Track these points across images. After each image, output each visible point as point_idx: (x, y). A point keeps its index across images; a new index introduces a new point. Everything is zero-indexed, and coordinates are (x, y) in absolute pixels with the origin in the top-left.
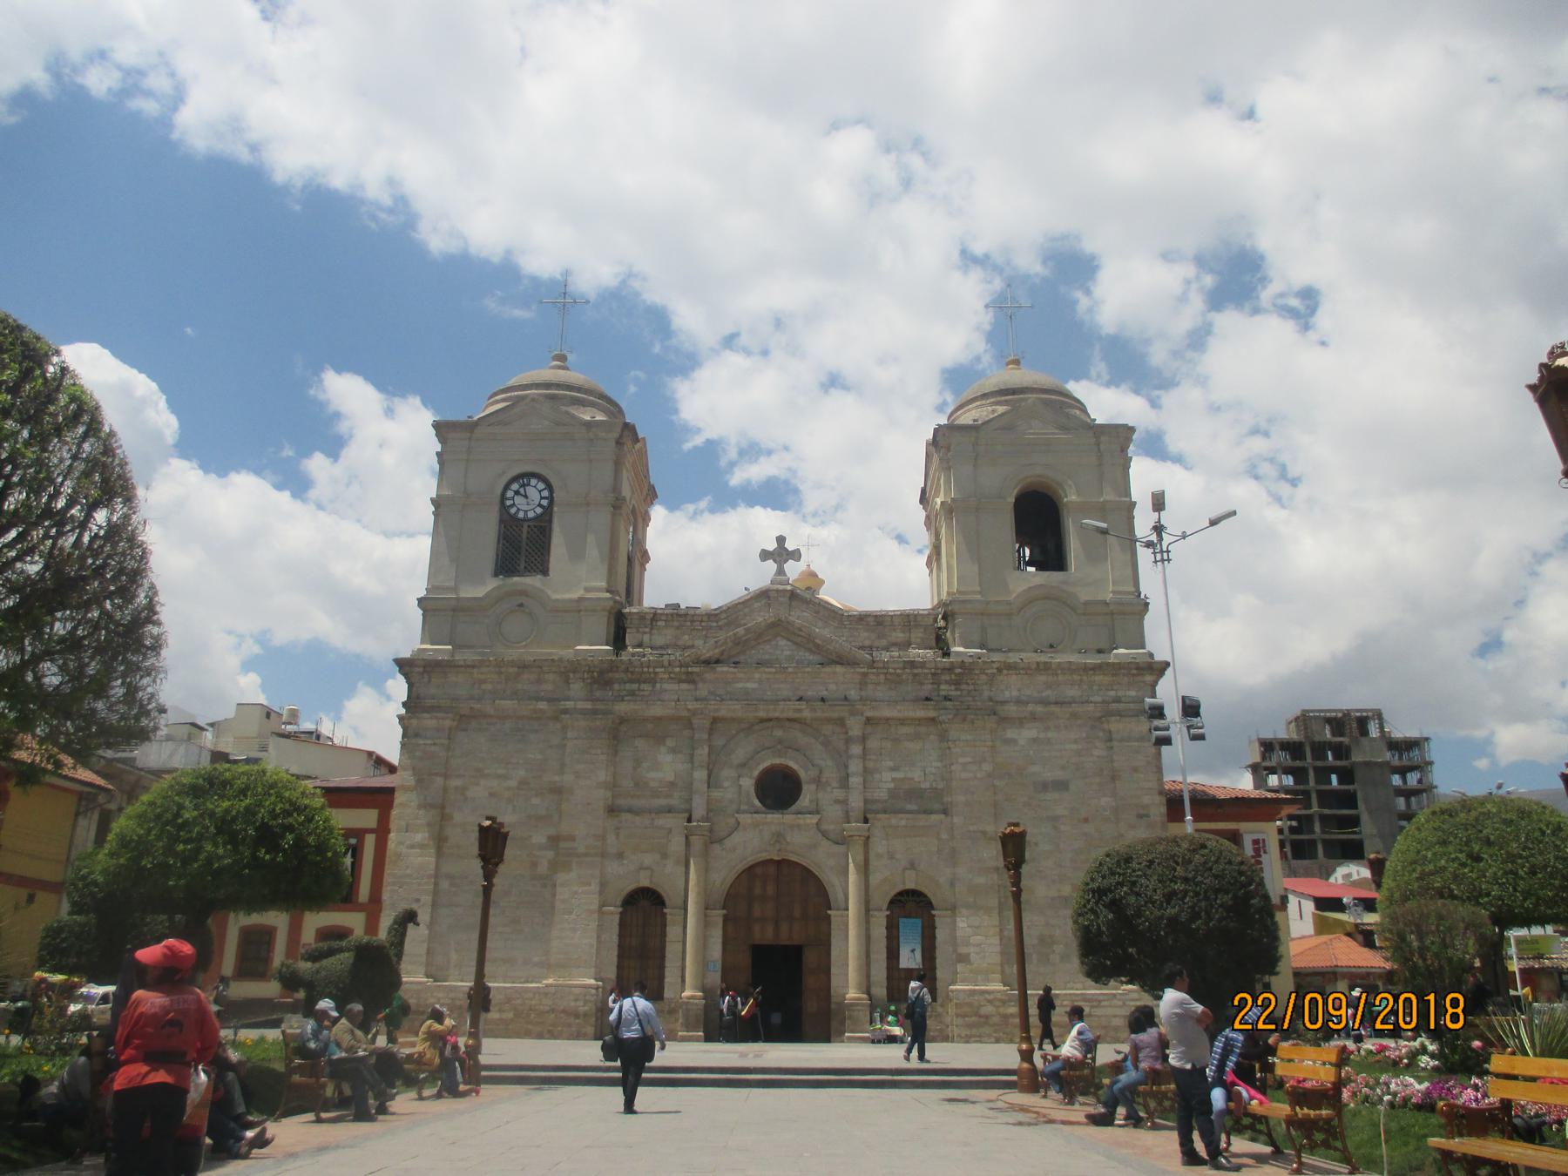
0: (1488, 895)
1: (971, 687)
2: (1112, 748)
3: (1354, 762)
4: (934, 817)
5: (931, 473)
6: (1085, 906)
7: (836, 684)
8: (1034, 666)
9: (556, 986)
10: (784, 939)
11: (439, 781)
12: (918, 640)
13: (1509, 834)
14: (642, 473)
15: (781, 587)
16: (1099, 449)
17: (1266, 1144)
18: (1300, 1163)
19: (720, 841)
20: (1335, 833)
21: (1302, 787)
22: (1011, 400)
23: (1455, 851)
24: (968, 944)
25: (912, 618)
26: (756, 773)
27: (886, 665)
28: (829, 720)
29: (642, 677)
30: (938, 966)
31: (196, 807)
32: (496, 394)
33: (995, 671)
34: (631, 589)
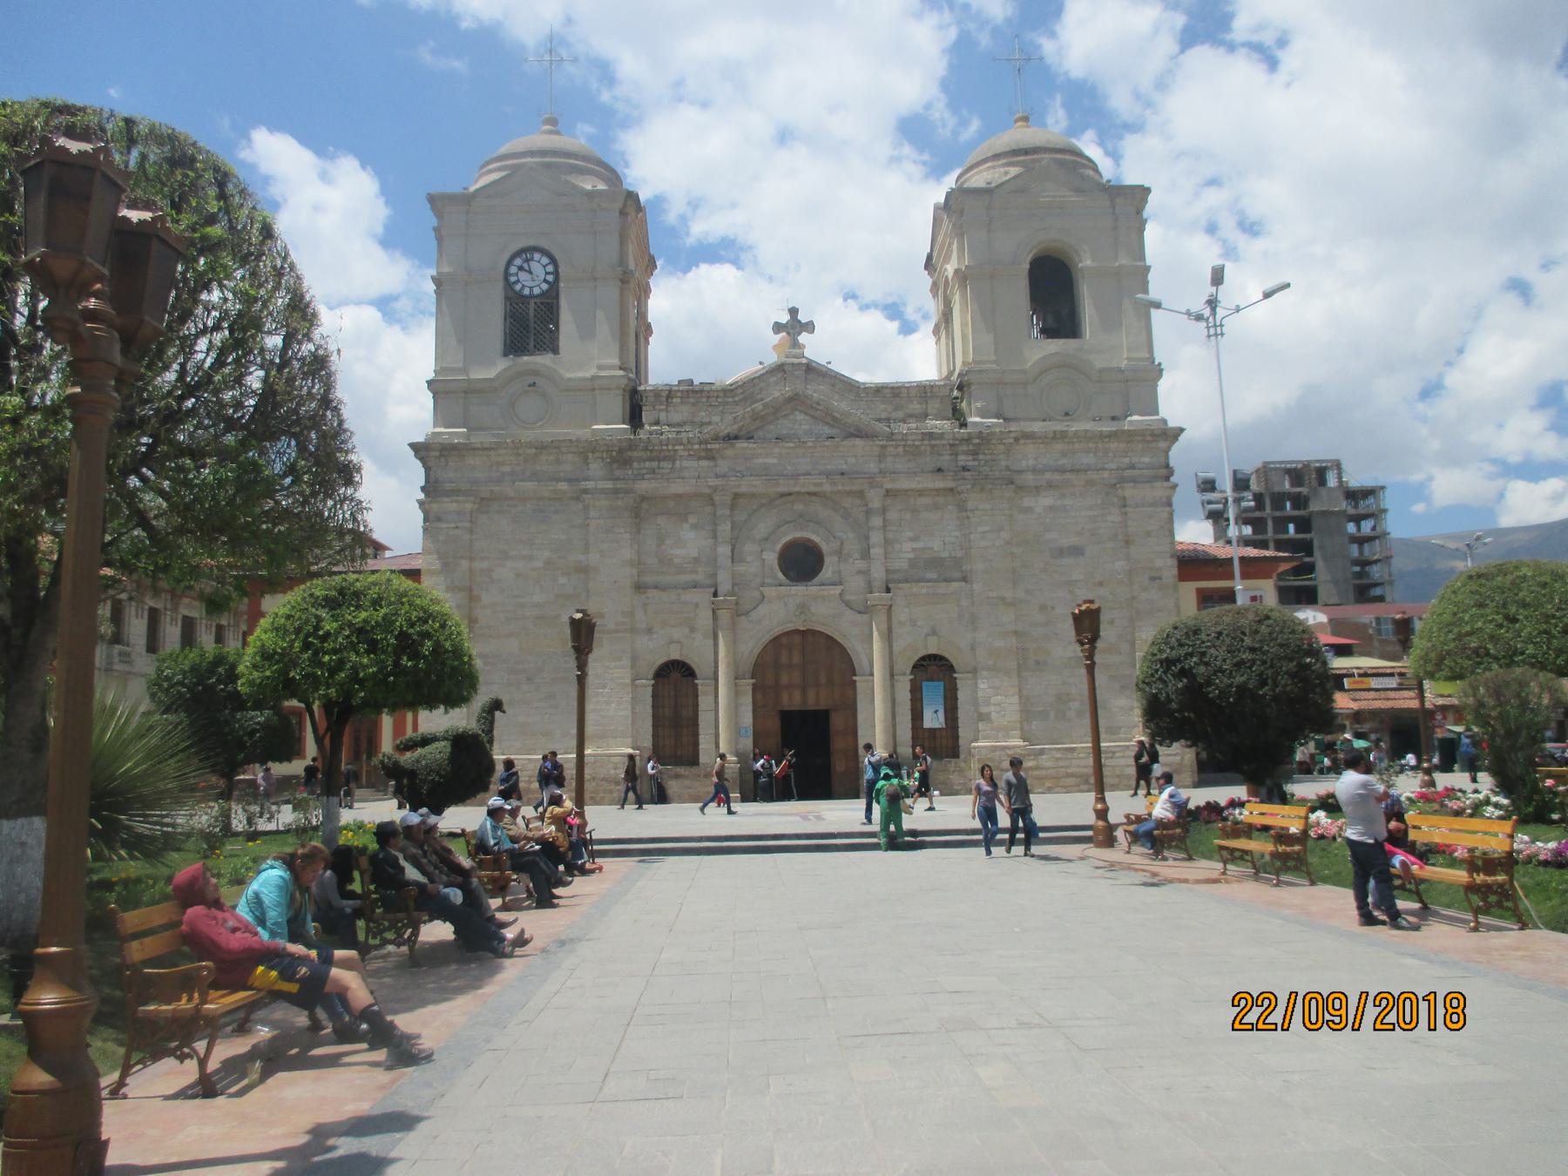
0: (1522, 653)
2: (1126, 514)
3: (1312, 512)
4: (955, 585)
5: (940, 239)
6: (1152, 675)
7: (855, 456)
8: (1051, 435)
9: (594, 755)
11: (465, 564)
12: (935, 412)
13: (1544, 595)
14: (644, 243)
15: (796, 361)
19: (747, 613)
20: (1289, 580)
22: (1024, 161)
23: (1492, 614)
26: (779, 547)
27: (904, 437)
28: (849, 493)
29: (661, 455)
31: (335, 618)
32: (488, 163)
33: (1012, 441)
34: (638, 365)
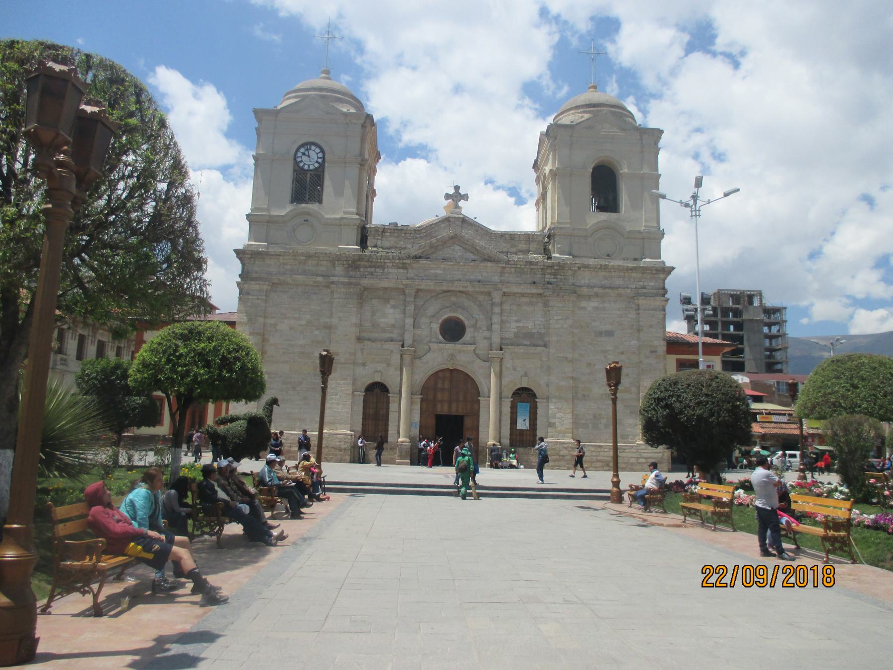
0: (860, 407)
1: (563, 277)
2: (639, 314)
4: (540, 349)
6: (649, 407)
8: (599, 267)
10: (454, 412)
11: (261, 320)
12: (534, 249)
13: (874, 374)
14: (374, 144)
15: (456, 216)
16: (642, 143)
17: (793, 544)
18: (828, 558)
19: (420, 358)
21: (714, 332)
22: (593, 111)
24: (554, 417)
25: (531, 237)
26: (440, 321)
27: (516, 263)
28: (482, 293)
29: (376, 264)
30: (538, 428)
33: (577, 269)
